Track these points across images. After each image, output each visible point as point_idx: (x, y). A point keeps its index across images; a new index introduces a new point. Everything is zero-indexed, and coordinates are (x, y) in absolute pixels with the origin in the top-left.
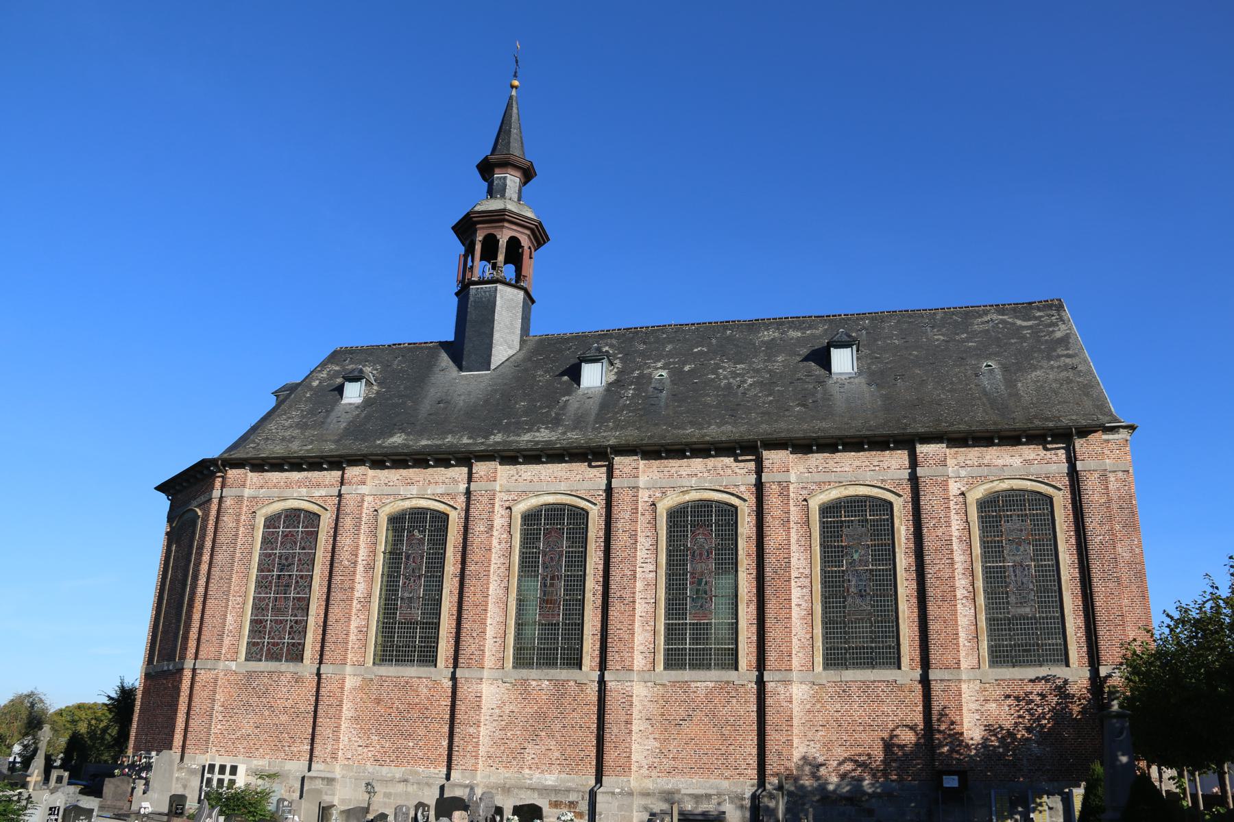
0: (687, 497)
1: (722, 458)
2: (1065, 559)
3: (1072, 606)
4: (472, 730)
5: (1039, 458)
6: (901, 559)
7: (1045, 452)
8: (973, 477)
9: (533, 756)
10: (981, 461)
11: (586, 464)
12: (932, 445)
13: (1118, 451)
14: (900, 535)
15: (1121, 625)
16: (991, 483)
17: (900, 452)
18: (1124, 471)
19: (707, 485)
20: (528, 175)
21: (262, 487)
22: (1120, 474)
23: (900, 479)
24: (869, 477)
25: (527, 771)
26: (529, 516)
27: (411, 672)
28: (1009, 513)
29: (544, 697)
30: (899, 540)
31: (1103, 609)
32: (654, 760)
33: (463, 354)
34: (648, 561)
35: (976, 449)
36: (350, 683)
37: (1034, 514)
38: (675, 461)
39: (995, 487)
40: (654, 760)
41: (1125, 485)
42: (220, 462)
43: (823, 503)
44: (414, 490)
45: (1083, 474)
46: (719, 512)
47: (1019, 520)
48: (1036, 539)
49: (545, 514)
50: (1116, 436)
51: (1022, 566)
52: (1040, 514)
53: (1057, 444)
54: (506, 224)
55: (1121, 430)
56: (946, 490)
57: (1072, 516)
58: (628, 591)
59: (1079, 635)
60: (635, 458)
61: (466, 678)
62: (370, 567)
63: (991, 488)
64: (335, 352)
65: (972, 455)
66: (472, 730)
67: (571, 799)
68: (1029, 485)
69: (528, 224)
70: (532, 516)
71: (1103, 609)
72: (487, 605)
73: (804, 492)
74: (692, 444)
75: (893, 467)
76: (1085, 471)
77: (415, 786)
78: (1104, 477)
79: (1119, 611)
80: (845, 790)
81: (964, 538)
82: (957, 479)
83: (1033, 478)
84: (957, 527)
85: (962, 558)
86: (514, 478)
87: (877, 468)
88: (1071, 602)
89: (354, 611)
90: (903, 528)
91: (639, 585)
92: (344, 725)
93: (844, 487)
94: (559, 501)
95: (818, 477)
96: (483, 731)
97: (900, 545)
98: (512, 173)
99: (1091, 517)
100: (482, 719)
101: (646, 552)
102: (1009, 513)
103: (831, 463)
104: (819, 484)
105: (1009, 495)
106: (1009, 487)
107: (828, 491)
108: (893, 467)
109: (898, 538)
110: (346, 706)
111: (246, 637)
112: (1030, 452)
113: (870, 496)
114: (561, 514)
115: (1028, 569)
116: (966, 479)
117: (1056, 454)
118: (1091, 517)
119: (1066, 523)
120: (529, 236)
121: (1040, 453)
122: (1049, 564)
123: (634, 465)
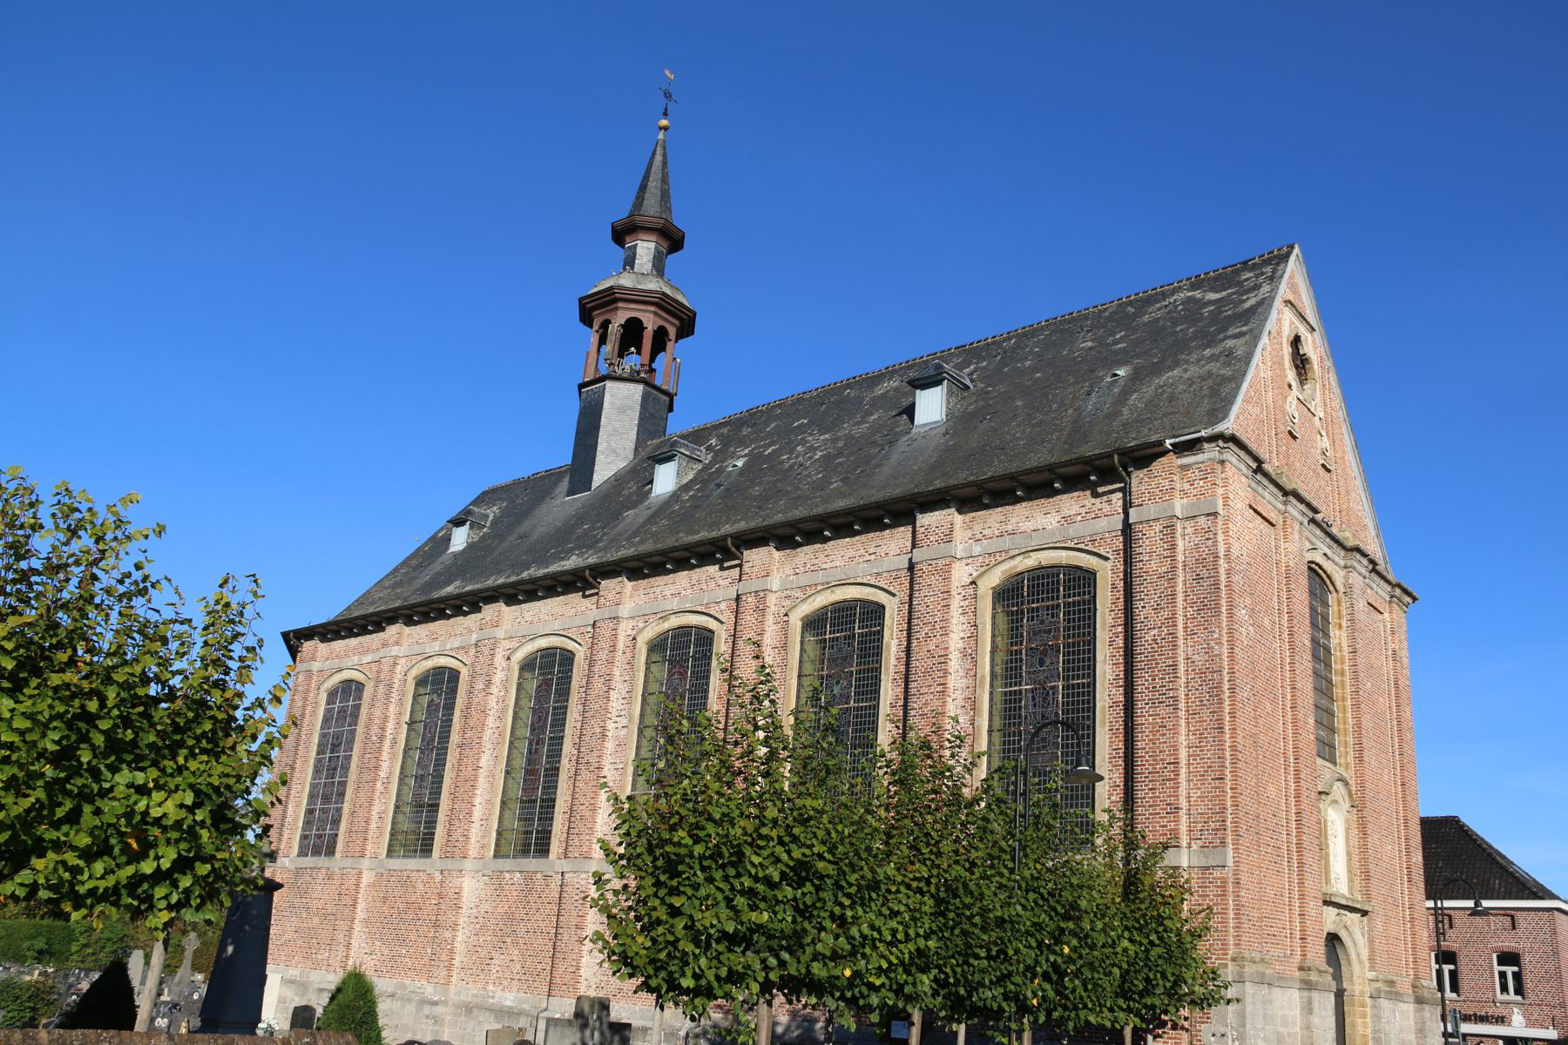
0: (667, 625)
1: (707, 568)
2: (1105, 673)
3: (1107, 750)
4: (448, 934)
5: (1083, 511)
6: (886, 690)
7: (1093, 500)
8: (990, 554)
9: (499, 968)
10: (1004, 527)
11: (580, 594)
12: (937, 513)
13: (1201, 482)
14: (889, 654)
15: (1172, 780)
16: (1011, 561)
17: (902, 528)
18: (1208, 515)
19: (688, 606)
20: (673, 240)
21: (327, 659)
22: (1202, 520)
23: (898, 570)
24: (862, 571)
25: (491, 987)
26: (1004, 593)
27: (413, 863)
28: (1034, 605)
29: (514, 894)
30: (888, 660)
31: (1147, 753)
32: (603, 978)
33: (1354, 429)
34: (622, 713)
35: (1000, 509)
36: (367, 878)
37: (1069, 603)
38: (661, 578)
39: (1017, 566)
40: (603, 978)
41: (1207, 539)
42: (292, 634)
43: (807, 616)
44: (436, 647)
45: (1138, 527)
46: (1033, 587)
47: (1048, 614)
48: (1069, 644)
49: (1028, 586)
50: (1200, 457)
51: (1044, 689)
52: (1079, 602)
53: (1112, 484)
54: (621, 305)
55: (1206, 445)
56: (947, 579)
57: (1122, 600)
58: (596, 753)
59: (1113, 798)
60: (620, 579)
61: (450, 870)
62: (394, 742)
63: (1011, 568)
64: (484, 493)
65: (992, 520)
66: (448, 934)
67: (520, 1025)
68: (1063, 557)
69: (666, 305)
70: (1013, 591)
71: (1147, 753)
72: (476, 780)
73: (787, 603)
74: (647, 557)
75: (892, 553)
76: (1141, 522)
77: (399, 1003)
78: (1169, 530)
79: (1171, 755)
80: (795, 1034)
81: (970, 651)
82: (970, 561)
83: (1072, 545)
84: (962, 635)
85: (963, 683)
86: (518, 620)
87: (873, 557)
88: (1108, 744)
89: (378, 794)
90: (894, 643)
91: (610, 745)
92: (358, 927)
93: (829, 591)
94: (551, 645)
95: (804, 580)
96: (460, 936)
97: (887, 669)
98: (644, 238)
99: (1143, 599)
100: (461, 921)
101: (622, 701)
102: (1034, 605)
103: (821, 556)
104: (803, 588)
105: (1048, 575)
106: (1036, 564)
107: (812, 598)
108: (892, 553)
109: (886, 658)
110: (361, 906)
111: (300, 829)
112: (1072, 504)
113: (859, 600)
114: (1053, 582)
115: (1054, 694)
116: (981, 558)
117: (1109, 501)
118: (1143, 599)
119: (1112, 613)
120: (655, 313)
121: (1086, 502)
122: (1083, 683)
123: (618, 589)
